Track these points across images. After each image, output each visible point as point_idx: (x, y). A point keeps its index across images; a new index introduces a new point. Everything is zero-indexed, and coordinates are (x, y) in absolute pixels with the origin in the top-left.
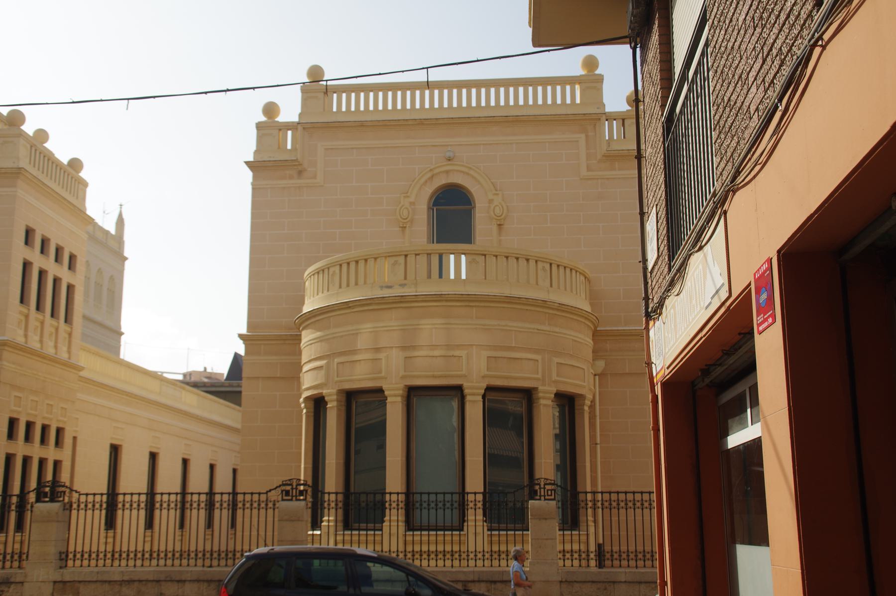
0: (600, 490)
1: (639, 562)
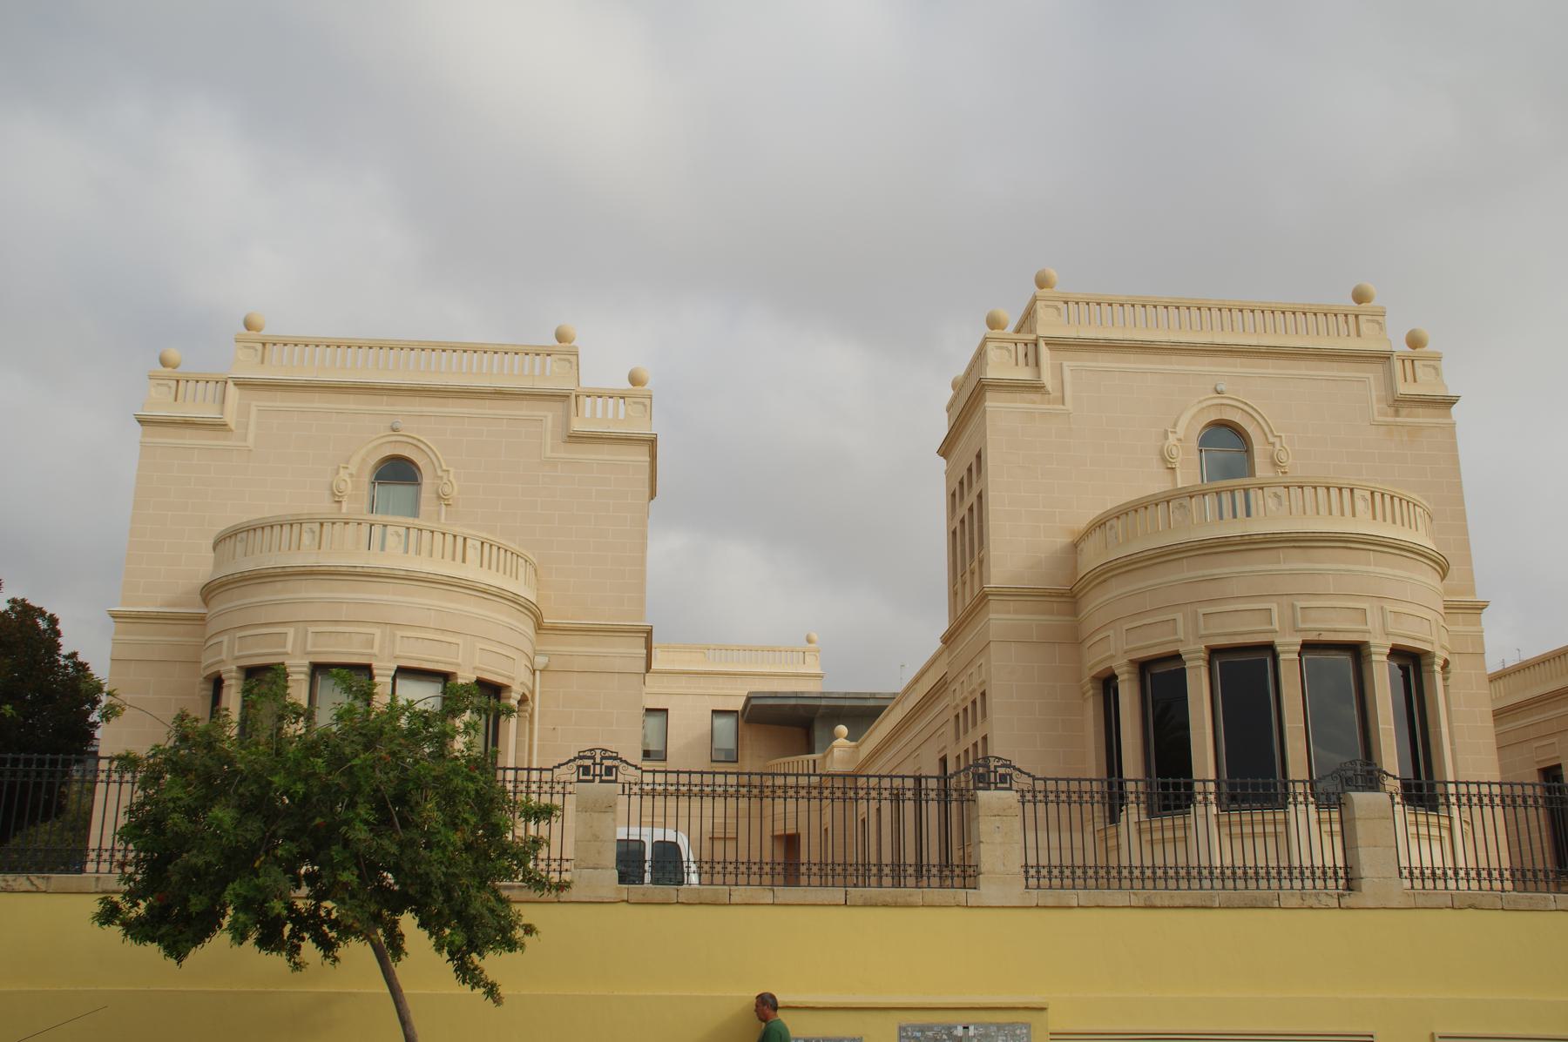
0: (511, 764)
1: (1077, 881)
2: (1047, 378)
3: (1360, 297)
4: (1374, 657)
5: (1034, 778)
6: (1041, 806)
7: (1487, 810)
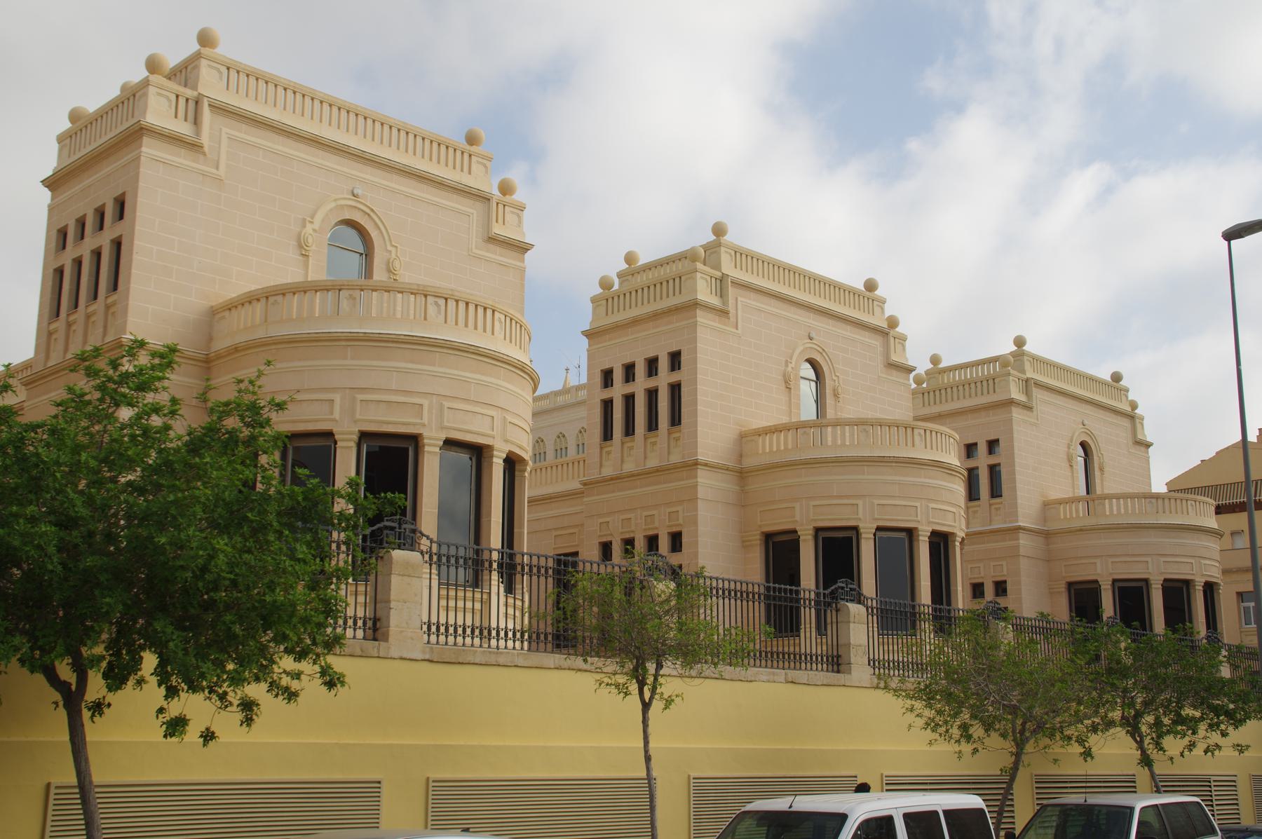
2: (205, 140)
3: (472, 139)
4: (427, 448)
5: (432, 541)
7: (542, 579)
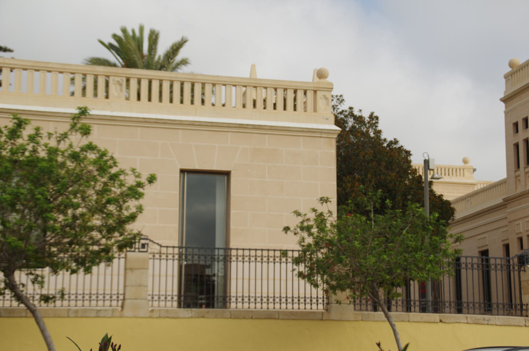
5: (161, 246)
6: (265, 264)
